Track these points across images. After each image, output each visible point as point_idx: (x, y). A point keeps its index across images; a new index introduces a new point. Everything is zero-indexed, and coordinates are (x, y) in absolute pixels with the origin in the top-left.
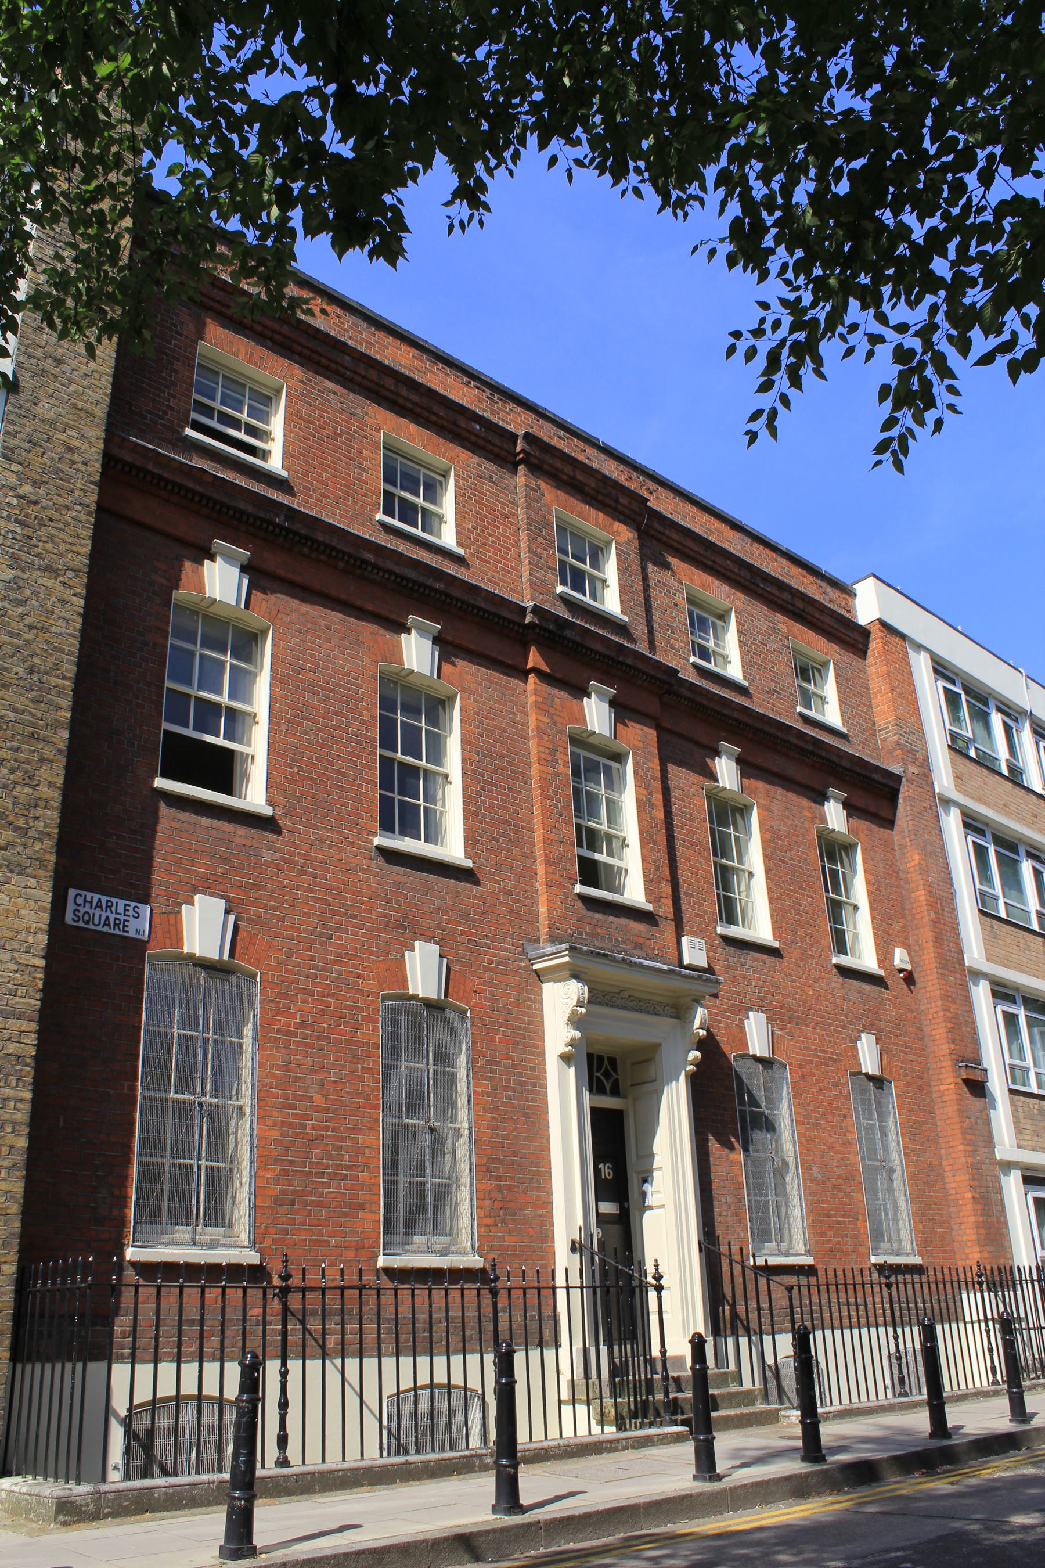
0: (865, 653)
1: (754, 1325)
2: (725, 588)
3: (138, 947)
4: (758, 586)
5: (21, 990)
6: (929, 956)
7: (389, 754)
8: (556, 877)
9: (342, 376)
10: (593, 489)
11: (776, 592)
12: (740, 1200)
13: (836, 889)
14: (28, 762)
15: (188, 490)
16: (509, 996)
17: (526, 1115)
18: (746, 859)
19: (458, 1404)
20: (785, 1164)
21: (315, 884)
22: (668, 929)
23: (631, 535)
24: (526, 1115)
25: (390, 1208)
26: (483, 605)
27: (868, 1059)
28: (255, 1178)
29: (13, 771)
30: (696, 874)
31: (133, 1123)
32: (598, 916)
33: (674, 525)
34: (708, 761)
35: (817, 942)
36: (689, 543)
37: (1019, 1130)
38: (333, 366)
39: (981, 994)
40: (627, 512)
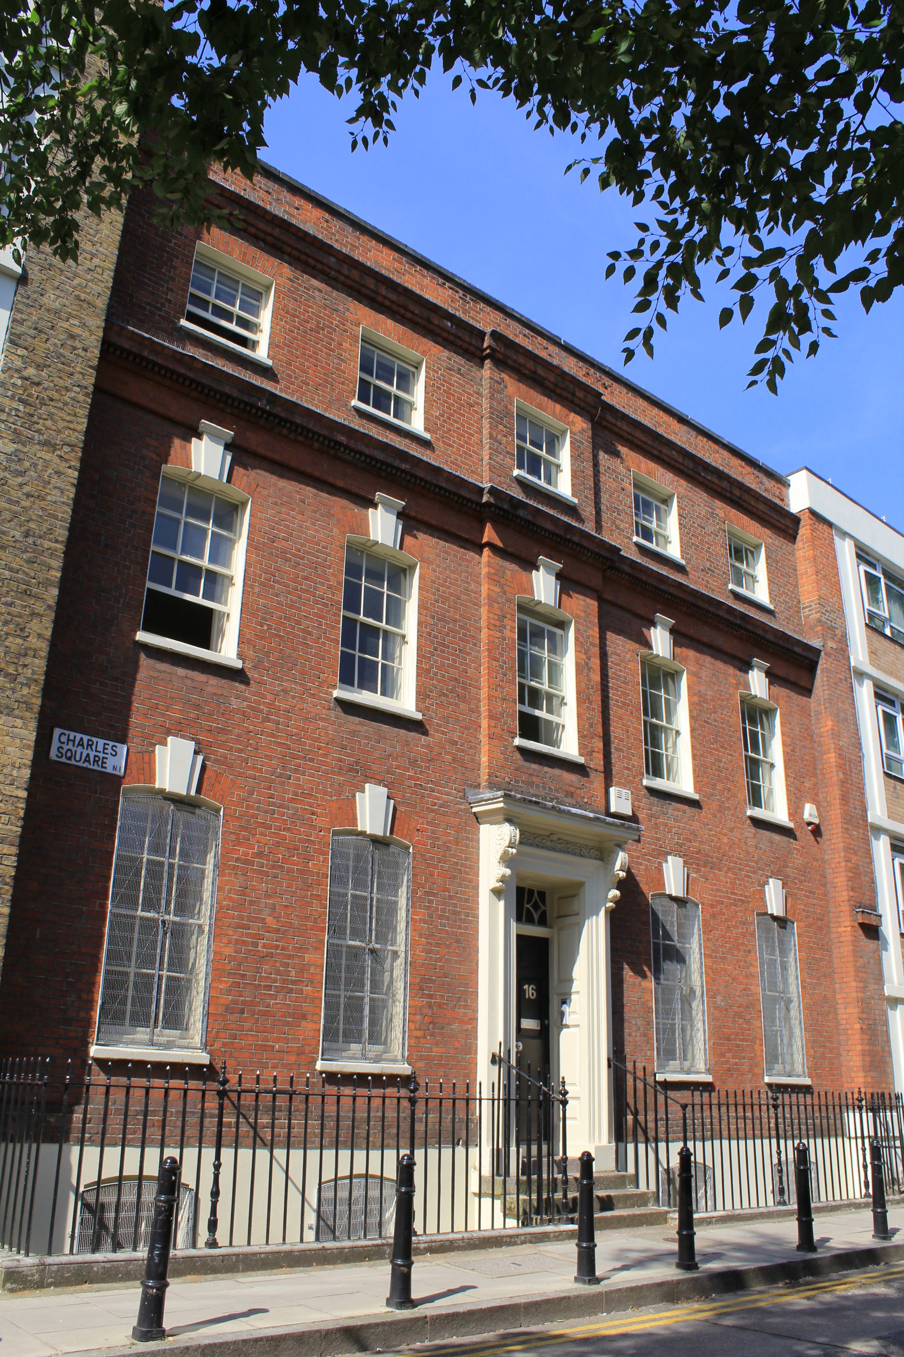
0: (795, 538)
1: (651, 1134)
2: (669, 476)
3: (115, 781)
4: (700, 474)
6: (836, 813)
8: (498, 730)
9: (327, 275)
10: (552, 383)
11: (716, 481)
12: (649, 1023)
13: (755, 748)
15: (179, 375)
17: (458, 941)
20: (692, 991)
21: (278, 730)
22: (597, 780)
23: (585, 426)
24: (458, 941)
25: (330, 1019)
26: (444, 485)
28: (209, 988)
30: (627, 731)
31: (102, 936)
32: (534, 766)
33: (625, 417)
34: (645, 630)
35: (735, 796)
36: (638, 434)
38: (319, 266)
40: (582, 404)
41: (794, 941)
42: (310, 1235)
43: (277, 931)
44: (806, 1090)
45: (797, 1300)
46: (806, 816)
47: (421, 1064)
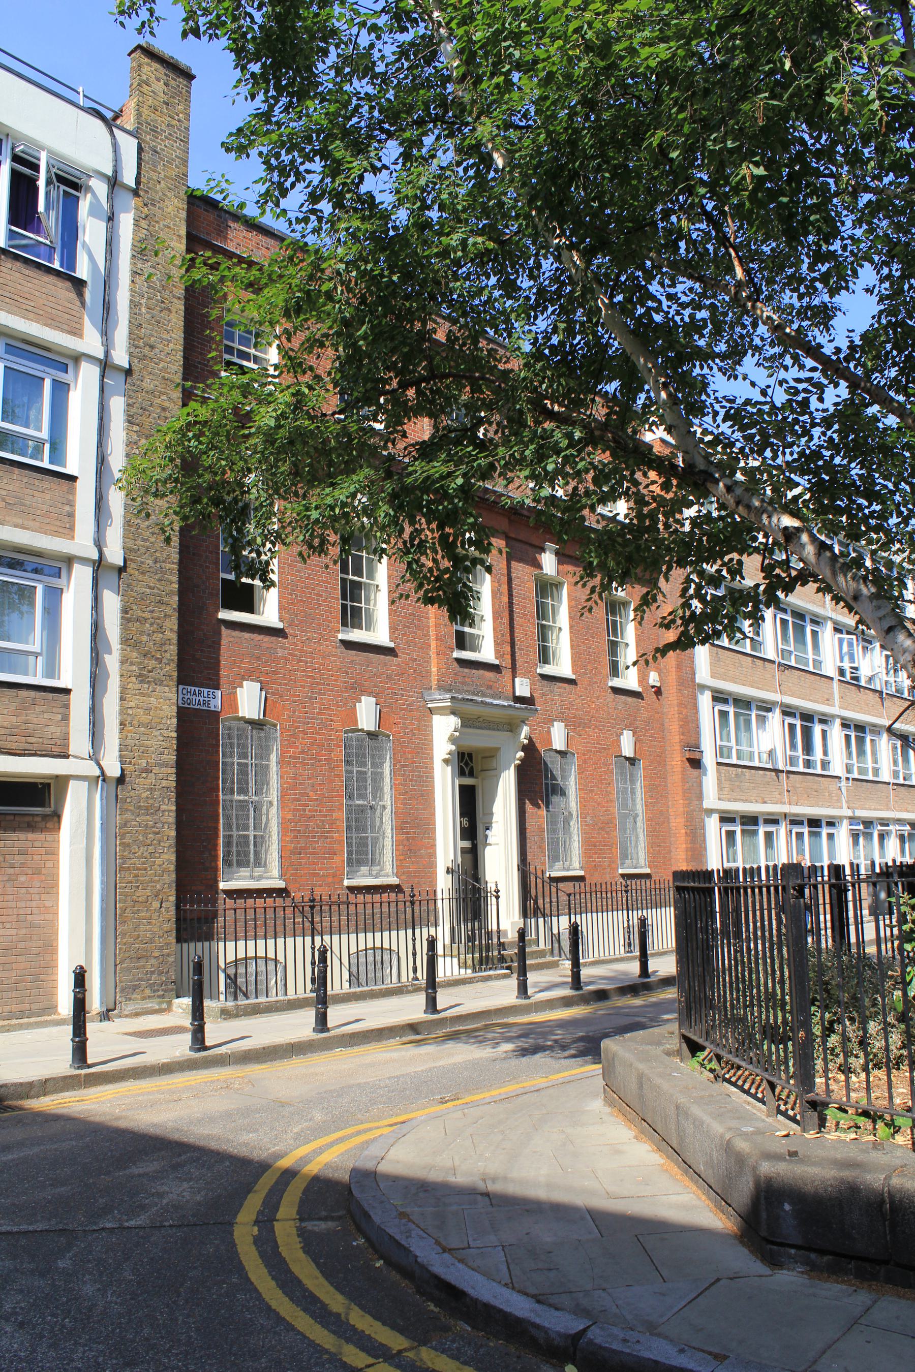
1: (547, 911)
3: (215, 715)
5: (166, 751)
6: (672, 677)
7: (345, 576)
12: (543, 839)
13: (615, 635)
14: (159, 618)
16: (413, 724)
17: (422, 795)
18: (558, 618)
19: (386, 958)
20: (570, 814)
21: (307, 667)
22: (507, 674)
24: (422, 795)
25: (350, 853)
27: (627, 745)
28: (281, 841)
29: (152, 625)
31: (218, 815)
32: (466, 670)
35: (600, 672)
37: (720, 788)
39: (705, 700)
41: (641, 773)
42: (346, 985)
43: (316, 800)
44: (648, 876)
45: (637, 1002)
46: (651, 682)
47: (404, 877)
